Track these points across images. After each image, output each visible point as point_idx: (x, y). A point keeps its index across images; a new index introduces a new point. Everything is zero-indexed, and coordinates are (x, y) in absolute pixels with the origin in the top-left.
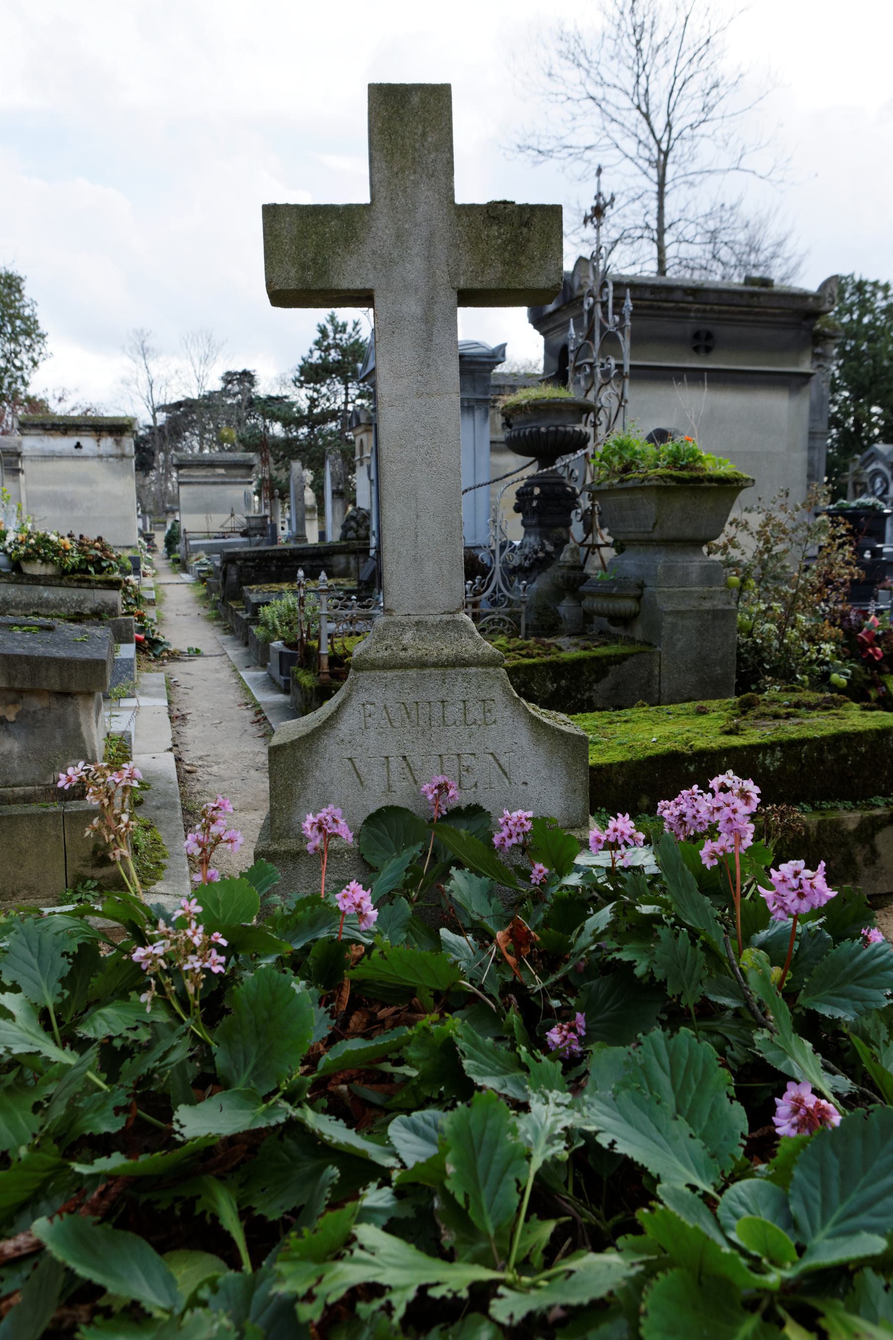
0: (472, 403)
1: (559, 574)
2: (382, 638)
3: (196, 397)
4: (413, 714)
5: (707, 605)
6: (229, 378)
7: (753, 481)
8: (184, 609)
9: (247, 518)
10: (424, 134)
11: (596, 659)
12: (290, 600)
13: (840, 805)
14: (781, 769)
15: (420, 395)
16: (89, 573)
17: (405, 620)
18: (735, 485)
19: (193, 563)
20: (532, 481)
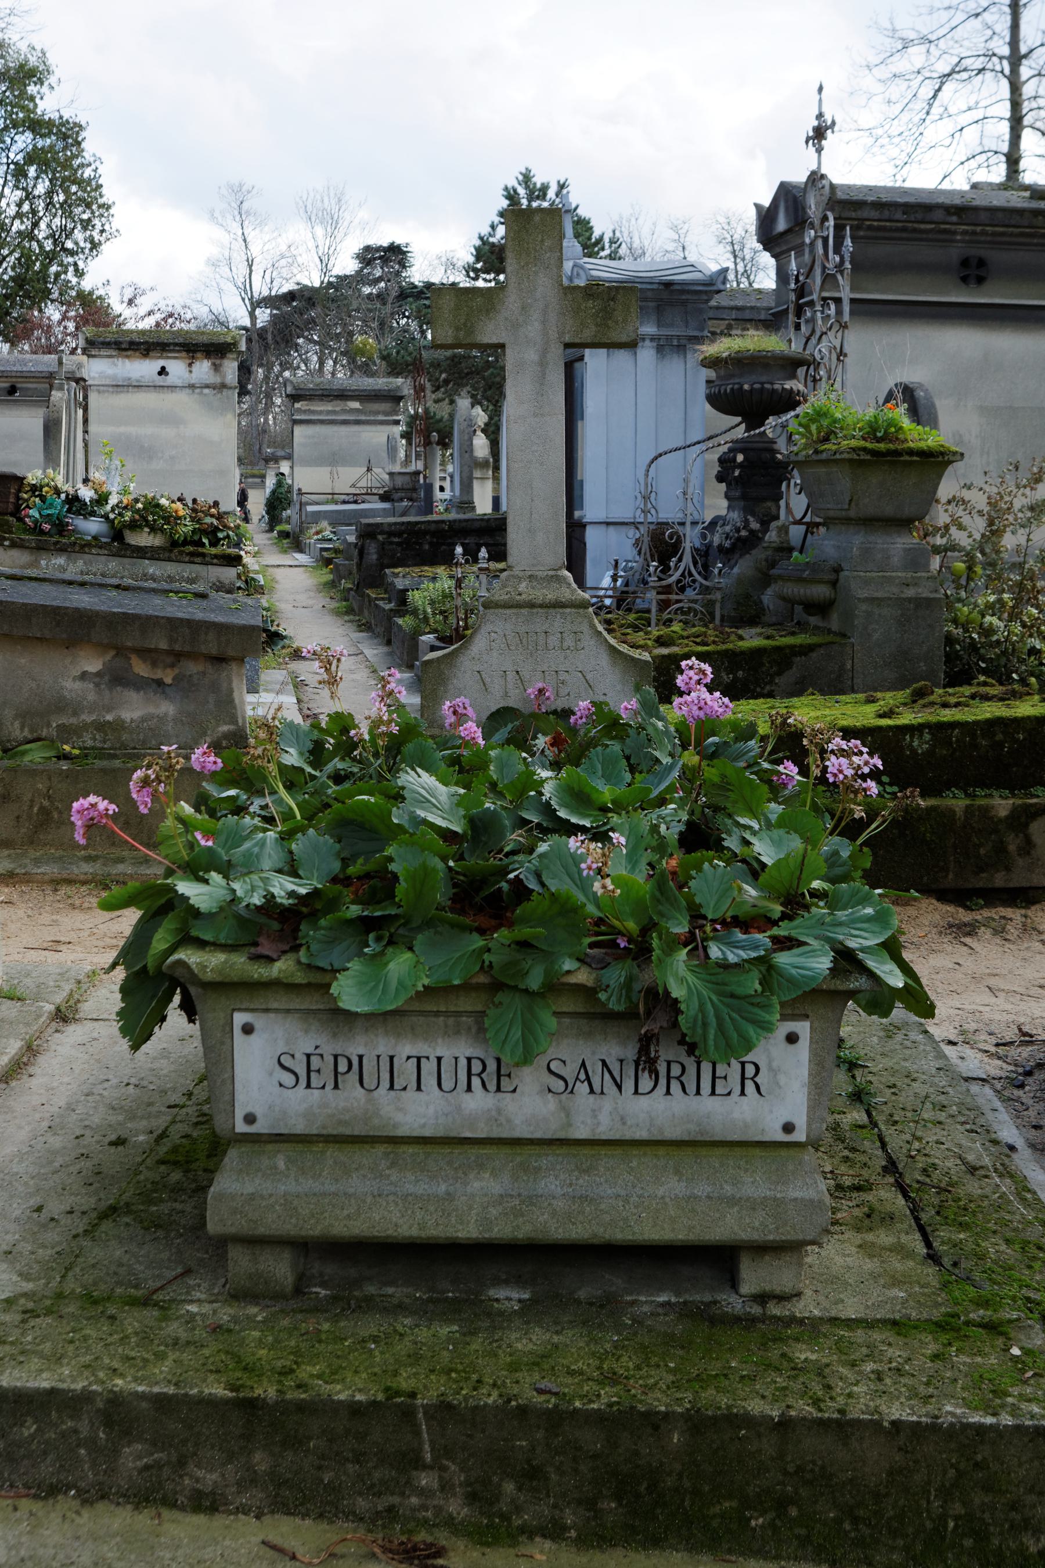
0: (683, 342)
1: (763, 556)
2: (504, 586)
3: (317, 284)
4: (524, 641)
5: (910, 592)
6: (368, 256)
7: (962, 455)
8: (303, 599)
9: (391, 474)
10: (542, 241)
11: (778, 649)
12: (446, 584)
13: (995, 793)
14: (930, 753)
15: (535, 415)
16: (203, 545)
17: (521, 574)
18: (940, 459)
19: (311, 538)
20: (738, 446)
